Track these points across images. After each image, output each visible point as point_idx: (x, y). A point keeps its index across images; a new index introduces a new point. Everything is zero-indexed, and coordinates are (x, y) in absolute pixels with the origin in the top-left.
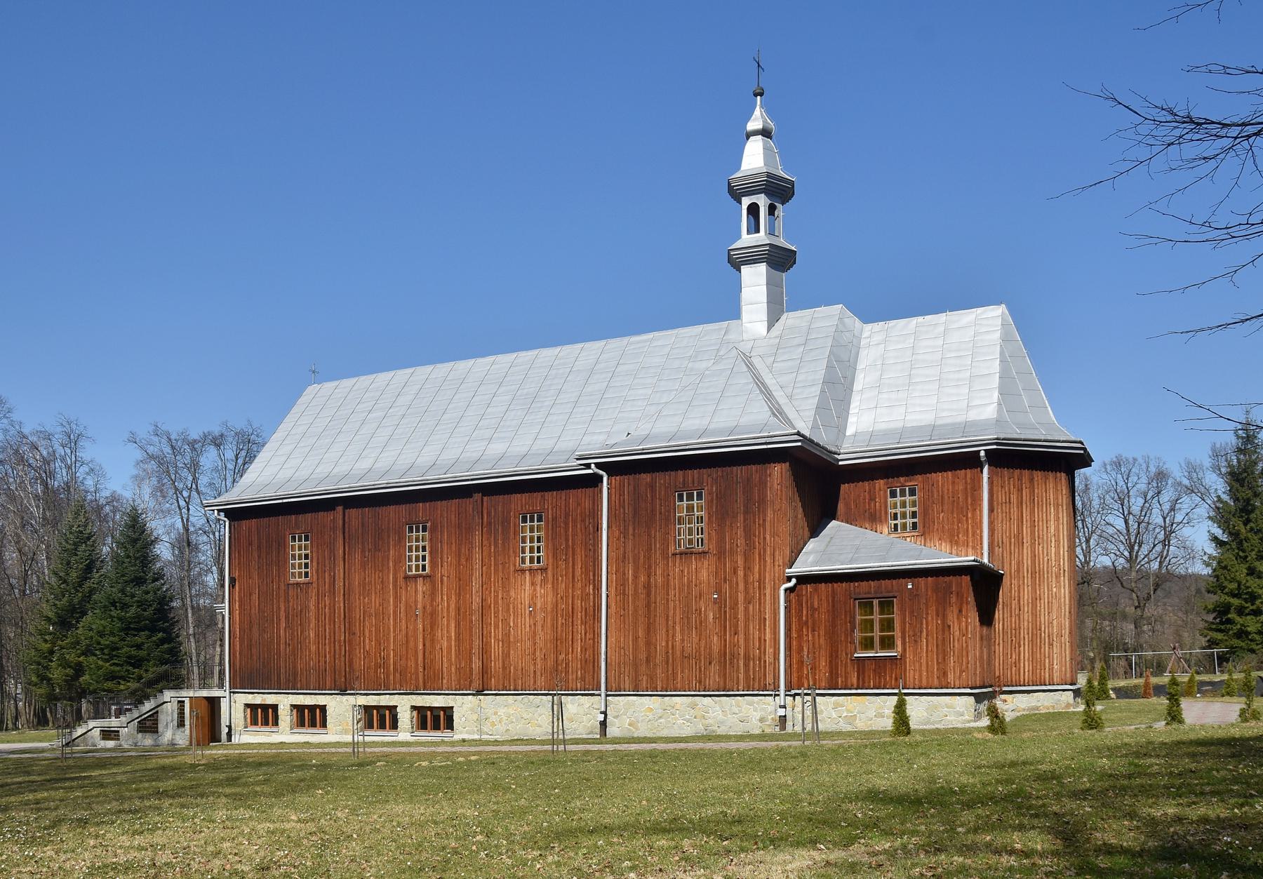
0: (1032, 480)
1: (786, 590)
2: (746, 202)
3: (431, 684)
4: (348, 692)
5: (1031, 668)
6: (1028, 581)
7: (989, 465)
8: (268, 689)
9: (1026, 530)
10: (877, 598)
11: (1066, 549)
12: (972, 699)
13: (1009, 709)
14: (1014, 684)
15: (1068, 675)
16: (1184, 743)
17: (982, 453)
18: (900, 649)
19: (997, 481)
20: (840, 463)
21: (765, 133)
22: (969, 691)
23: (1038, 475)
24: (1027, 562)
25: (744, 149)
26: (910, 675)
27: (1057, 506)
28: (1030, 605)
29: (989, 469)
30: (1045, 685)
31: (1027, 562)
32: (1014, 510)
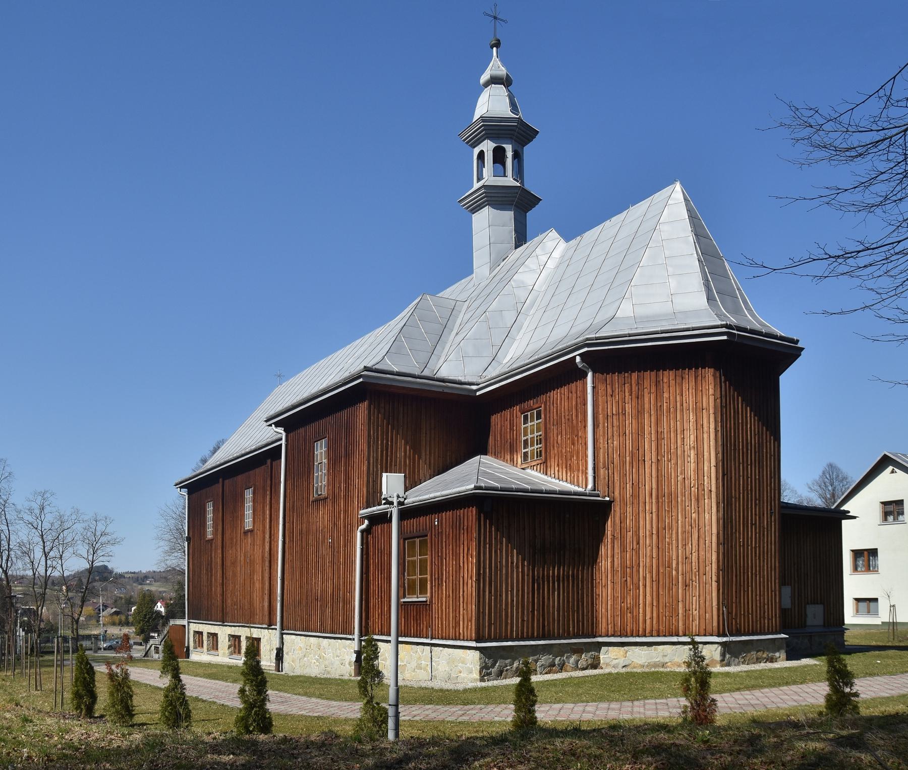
0: (657, 383)
1: (362, 532)
2: (476, 151)
3: (248, 620)
4: (225, 624)
5: (655, 615)
6: (651, 505)
7: (594, 372)
8: (231, 622)
9: (649, 446)
10: (418, 537)
11: (713, 463)
12: (476, 655)
13: (618, 664)
14: (702, 632)
15: (715, 624)
16: (796, 725)
17: (578, 359)
18: (429, 594)
19: (601, 388)
20: (478, 394)
21: (504, 81)
22: (473, 644)
23: (668, 376)
24: (649, 484)
25: (478, 100)
26: (436, 623)
27: (699, 410)
28: (655, 537)
29: (593, 377)
30: (678, 635)
31: (649, 484)
32: (630, 425)
